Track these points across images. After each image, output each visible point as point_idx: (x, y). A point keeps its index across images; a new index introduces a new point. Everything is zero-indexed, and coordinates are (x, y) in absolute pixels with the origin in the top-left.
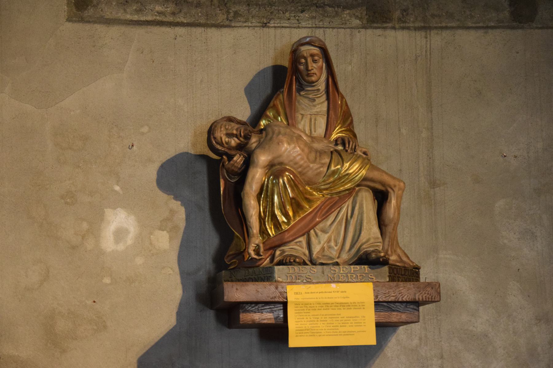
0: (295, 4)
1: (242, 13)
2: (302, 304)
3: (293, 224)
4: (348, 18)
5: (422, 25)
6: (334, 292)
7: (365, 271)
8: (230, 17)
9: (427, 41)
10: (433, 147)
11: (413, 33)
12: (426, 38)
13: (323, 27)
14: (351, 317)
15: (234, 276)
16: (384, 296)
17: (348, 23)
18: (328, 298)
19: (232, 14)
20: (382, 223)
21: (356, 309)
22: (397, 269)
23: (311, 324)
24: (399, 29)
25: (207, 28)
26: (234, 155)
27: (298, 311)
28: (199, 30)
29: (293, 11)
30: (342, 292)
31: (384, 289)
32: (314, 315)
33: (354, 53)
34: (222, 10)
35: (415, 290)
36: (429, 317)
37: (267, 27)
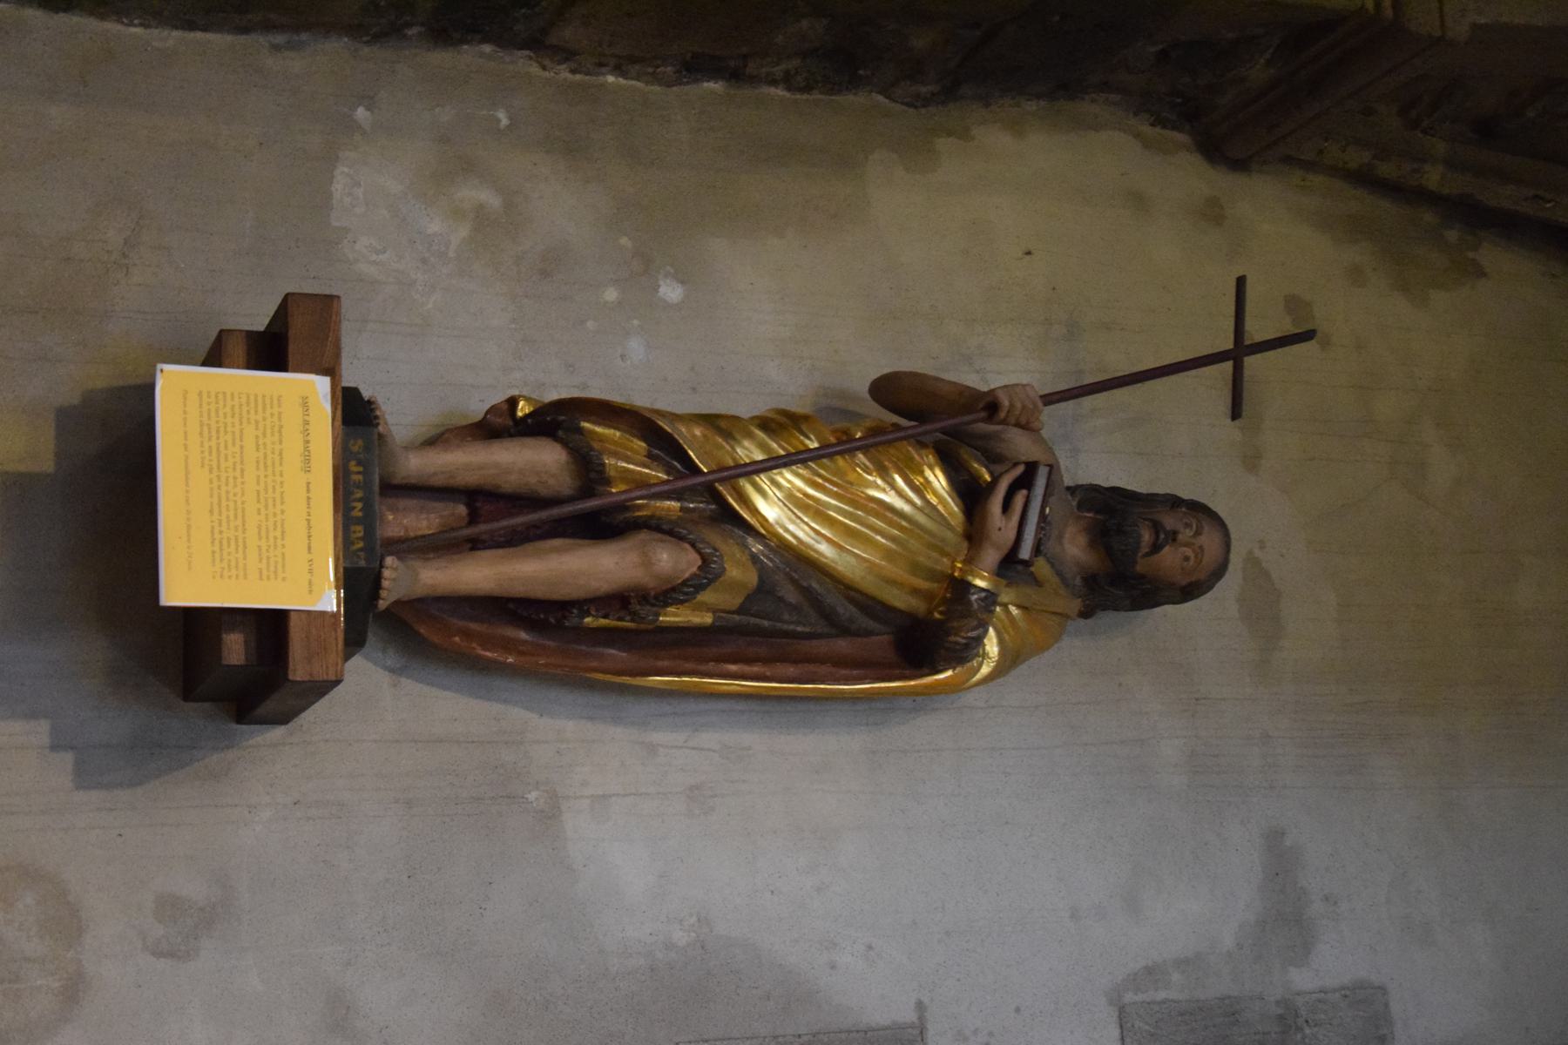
0: (213, 524)
6: (311, 561)
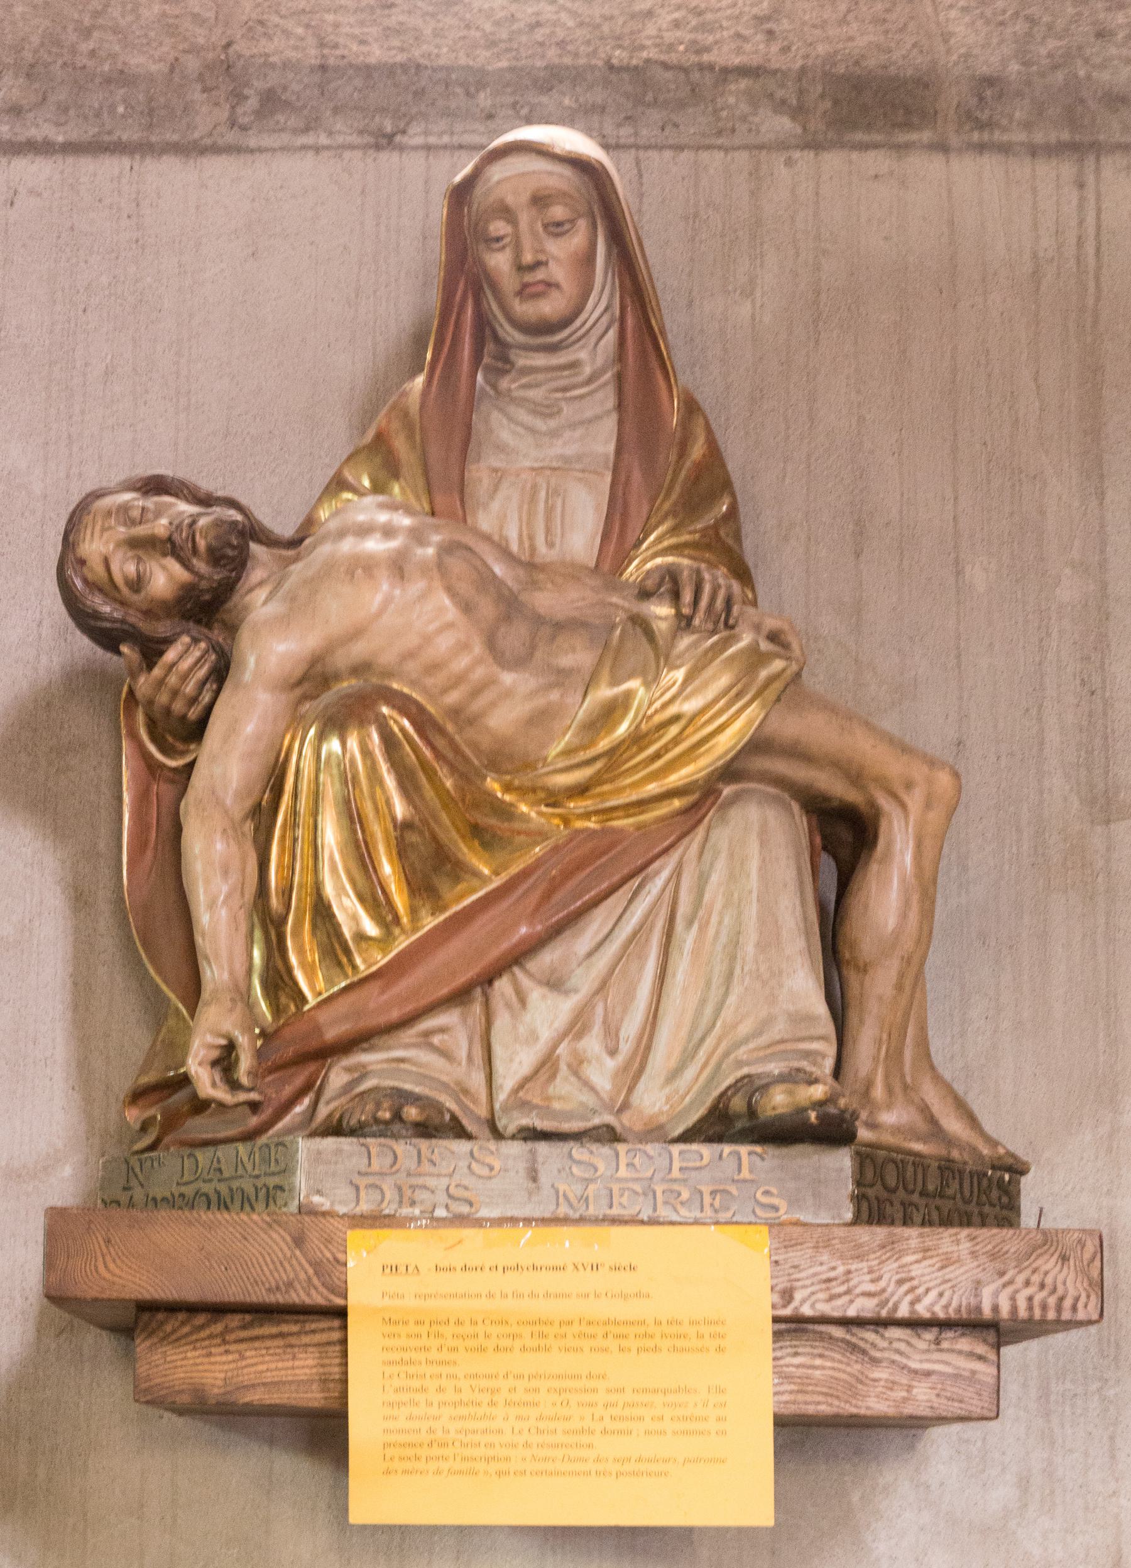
1: (294, 98)
2: (417, 1323)
3: (408, 947)
4: (744, 107)
5: (1066, 136)
7: (740, 1171)
8: (245, 114)
9: (1082, 200)
10: (1108, 646)
11: (1022, 168)
12: (1081, 186)
13: (637, 147)
14: (656, 1391)
15: (142, 1185)
16: (821, 1290)
17: (742, 128)
18: (547, 1295)
19: (253, 103)
20: (847, 955)
21: (683, 1350)
22: (900, 1166)
23: (461, 1418)
24: (960, 151)
25: (143, 157)
26: (168, 642)
27: (396, 1356)
28: (111, 166)
29: (508, 85)
30: (617, 1268)
31: (825, 1258)
32: (476, 1376)
33: (765, 246)
34: (211, 89)
35: (979, 1266)
36: (1068, 1385)
37: (393, 149)
